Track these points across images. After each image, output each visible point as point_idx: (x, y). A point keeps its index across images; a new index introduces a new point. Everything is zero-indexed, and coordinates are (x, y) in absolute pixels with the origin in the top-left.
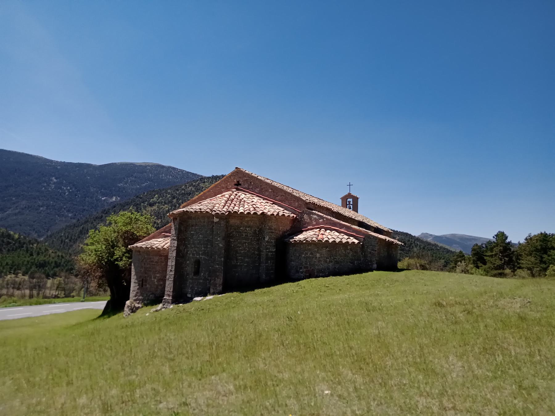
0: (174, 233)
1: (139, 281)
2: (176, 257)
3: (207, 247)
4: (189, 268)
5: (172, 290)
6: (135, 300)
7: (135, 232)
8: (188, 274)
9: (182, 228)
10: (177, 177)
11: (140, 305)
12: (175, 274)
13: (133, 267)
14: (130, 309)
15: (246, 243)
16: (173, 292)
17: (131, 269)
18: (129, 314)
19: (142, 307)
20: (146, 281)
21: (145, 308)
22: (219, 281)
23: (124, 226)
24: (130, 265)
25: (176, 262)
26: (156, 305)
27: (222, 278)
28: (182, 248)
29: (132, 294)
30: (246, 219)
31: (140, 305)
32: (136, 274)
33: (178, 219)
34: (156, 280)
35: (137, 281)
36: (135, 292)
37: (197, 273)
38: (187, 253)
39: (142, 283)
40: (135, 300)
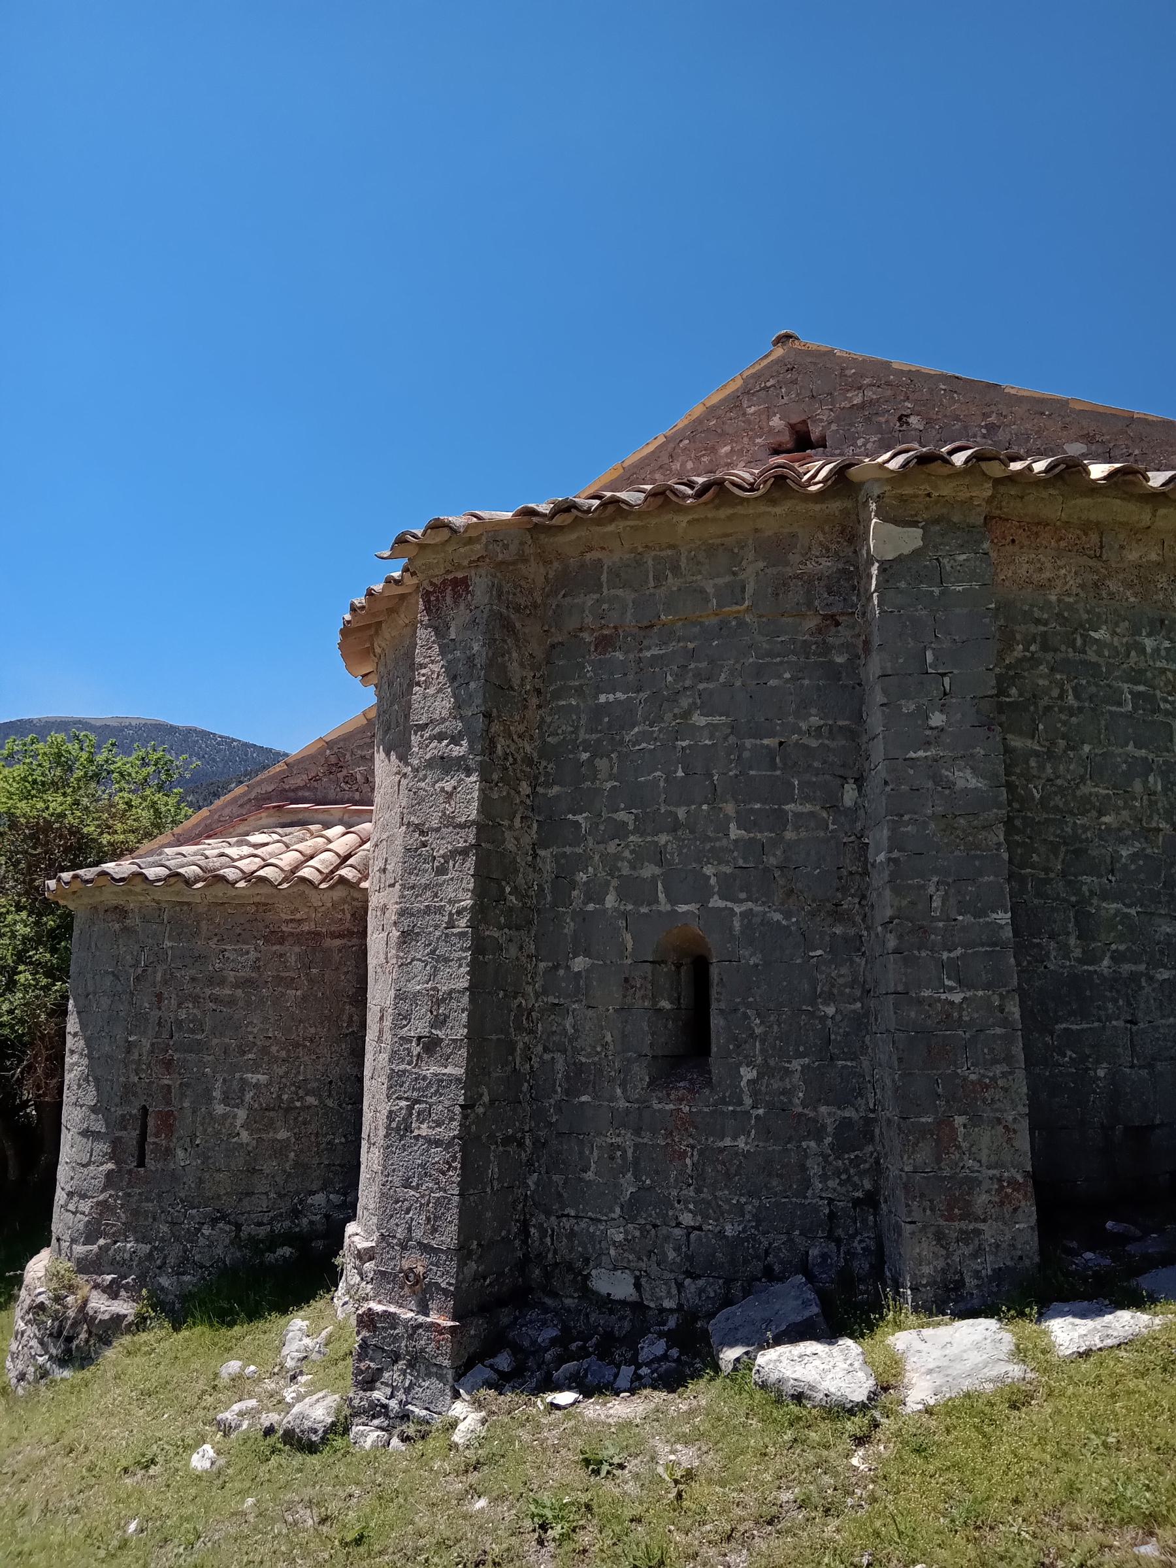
0: (443, 705)
1: (117, 1124)
2: (480, 913)
3: (779, 820)
4: (604, 1020)
5: (448, 1237)
6: (85, 1266)
7: (90, 829)
8: (578, 1077)
9: (515, 671)
10: (214, 760)
11: (124, 1307)
12: (473, 1079)
13: (72, 1024)
14: (56, 1335)
15: (1147, 767)
16: (463, 1251)
17: (62, 1034)
18: (44, 1374)
19: (141, 1323)
20: (168, 1122)
21: (159, 1338)
22: (996, 1148)
23: (27, 796)
24: (60, 1012)
25: (476, 968)
26: (254, 1314)
27: (1016, 1113)
28: (518, 838)
29: (65, 1219)
30: (1132, 556)
31: (124, 1307)
32: (95, 1077)
33: (480, 584)
34: (242, 1114)
35: (99, 1126)
36: (85, 1206)
37: (689, 1048)
38: (563, 879)
39: (136, 1140)
40: (85, 1266)
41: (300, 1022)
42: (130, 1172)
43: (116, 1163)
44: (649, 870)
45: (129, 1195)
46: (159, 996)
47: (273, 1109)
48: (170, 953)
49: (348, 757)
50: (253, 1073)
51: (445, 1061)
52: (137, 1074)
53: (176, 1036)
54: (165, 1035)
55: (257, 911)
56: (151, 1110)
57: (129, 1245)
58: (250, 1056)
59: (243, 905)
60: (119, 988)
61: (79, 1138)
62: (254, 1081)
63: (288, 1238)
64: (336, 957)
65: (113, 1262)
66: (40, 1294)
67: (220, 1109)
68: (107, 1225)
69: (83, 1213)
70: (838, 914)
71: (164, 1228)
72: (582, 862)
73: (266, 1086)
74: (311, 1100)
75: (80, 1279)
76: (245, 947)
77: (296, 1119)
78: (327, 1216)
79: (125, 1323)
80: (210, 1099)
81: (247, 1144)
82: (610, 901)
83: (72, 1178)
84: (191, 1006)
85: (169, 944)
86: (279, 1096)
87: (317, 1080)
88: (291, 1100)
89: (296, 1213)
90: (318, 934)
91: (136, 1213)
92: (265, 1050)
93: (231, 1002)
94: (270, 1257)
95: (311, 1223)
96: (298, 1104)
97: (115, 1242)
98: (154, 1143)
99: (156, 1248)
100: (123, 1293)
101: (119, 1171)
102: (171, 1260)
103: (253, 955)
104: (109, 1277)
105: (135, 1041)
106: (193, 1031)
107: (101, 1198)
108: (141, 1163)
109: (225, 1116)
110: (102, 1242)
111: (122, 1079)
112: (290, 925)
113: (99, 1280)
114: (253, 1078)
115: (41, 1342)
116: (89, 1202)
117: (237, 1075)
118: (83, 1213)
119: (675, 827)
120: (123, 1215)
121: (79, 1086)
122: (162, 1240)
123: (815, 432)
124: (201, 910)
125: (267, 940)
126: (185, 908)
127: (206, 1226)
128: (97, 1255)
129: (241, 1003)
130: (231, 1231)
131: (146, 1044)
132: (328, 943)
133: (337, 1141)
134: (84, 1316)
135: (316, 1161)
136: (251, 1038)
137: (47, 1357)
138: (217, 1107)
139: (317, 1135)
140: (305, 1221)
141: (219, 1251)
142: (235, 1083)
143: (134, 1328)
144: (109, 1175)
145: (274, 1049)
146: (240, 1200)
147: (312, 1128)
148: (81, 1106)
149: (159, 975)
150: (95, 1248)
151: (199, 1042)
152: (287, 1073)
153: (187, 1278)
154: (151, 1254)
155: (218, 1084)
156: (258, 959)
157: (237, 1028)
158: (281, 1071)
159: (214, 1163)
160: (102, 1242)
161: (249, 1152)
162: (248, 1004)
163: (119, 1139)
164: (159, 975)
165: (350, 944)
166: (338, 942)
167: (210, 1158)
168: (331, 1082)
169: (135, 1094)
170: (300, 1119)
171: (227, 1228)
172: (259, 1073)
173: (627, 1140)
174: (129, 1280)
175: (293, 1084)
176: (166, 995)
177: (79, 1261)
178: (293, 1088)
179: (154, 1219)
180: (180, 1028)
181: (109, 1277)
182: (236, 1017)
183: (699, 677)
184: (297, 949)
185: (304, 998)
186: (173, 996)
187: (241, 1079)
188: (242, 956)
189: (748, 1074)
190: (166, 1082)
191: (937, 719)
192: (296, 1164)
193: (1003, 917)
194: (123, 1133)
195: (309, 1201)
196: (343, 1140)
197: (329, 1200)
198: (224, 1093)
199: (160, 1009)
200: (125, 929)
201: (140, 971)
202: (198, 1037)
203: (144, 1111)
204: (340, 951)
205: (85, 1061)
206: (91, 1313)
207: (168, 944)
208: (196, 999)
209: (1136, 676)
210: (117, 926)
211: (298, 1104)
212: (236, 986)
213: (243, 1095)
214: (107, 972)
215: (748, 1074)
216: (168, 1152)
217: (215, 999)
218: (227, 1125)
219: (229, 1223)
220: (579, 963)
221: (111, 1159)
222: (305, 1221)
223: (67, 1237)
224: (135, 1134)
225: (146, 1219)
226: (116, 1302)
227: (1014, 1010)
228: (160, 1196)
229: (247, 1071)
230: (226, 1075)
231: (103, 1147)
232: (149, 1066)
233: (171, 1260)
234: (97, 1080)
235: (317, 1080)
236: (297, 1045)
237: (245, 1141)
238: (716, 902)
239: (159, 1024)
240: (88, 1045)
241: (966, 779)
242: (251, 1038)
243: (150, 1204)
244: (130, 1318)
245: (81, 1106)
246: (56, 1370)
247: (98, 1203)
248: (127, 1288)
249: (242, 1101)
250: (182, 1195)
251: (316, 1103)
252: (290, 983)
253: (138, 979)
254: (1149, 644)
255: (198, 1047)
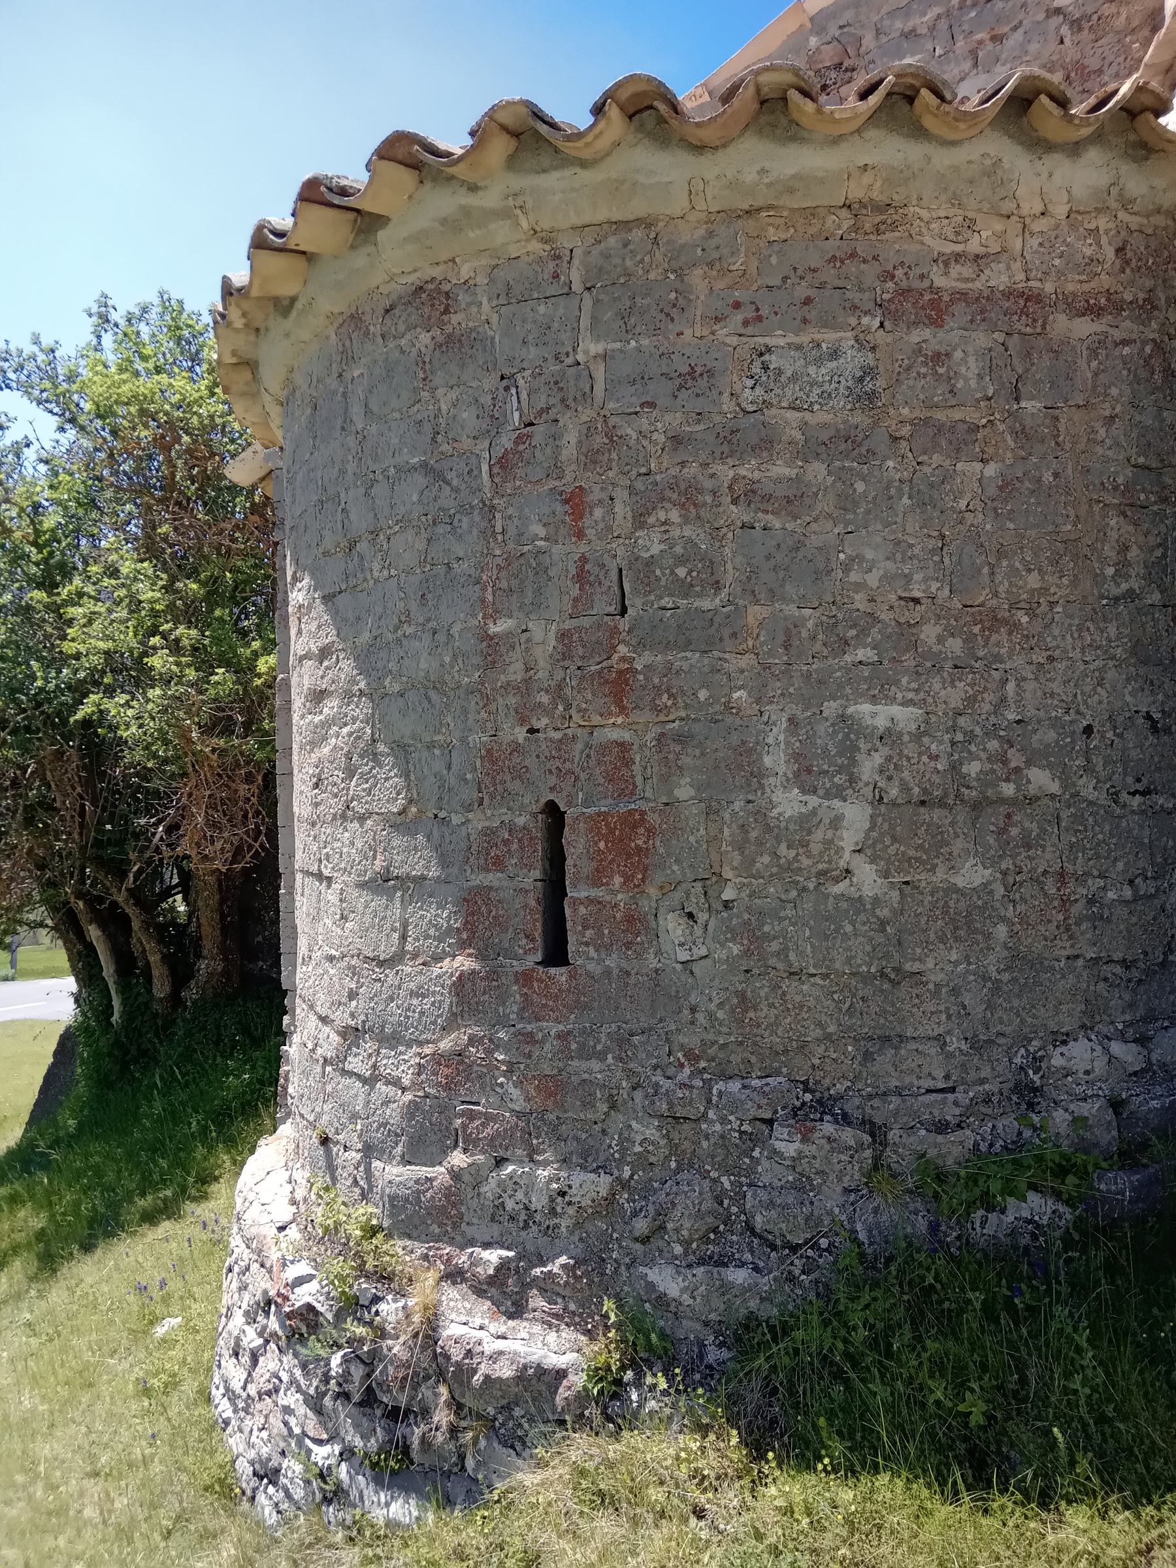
20: (629, 845)
32: (394, 741)
34: (855, 816)
35: (418, 861)
36: (403, 1064)
39: (540, 895)
41: (1001, 554)
42: (525, 978)
43: (481, 956)
45: (530, 1038)
46: (575, 502)
47: (942, 803)
48: (599, 372)
49: (869, 41)
50: (874, 700)
52: (522, 721)
53: (635, 605)
54: (604, 604)
55: (855, 228)
56: (570, 814)
57: (543, 1173)
58: (862, 654)
59: (811, 213)
60: (447, 500)
61: (360, 899)
62: (881, 723)
63: (1022, 1165)
64: (1085, 369)
65: (497, 1212)
66: (300, 1281)
67: (788, 803)
68: (472, 1116)
69: (396, 1082)
71: (647, 1131)
73: (917, 736)
74: (1041, 779)
75: (402, 1253)
76: (828, 337)
77: (1001, 832)
78: (1116, 1105)
79: (562, 1393)
80: (756, 777)
81: (876, 901)
83: (353, 995)
84: (675, 516)
85: (596, 348)
86: (954, 767)
87: (1056, 723)
88: (987, 780)
89: (1028, 1095)
90: (1032, 298)
91: (554, 1088)
92: (906, 635)
93: (794, 501)
94: (990, 1226)
95: (1078, 1121)
96: (1008, 789)
97: (500, 1162)
98: (590, 901)
99: (625, 1185)
100: (537, 1301)
101: (493, 974)
102: (682, 1222)
103: (852, 360)
104: (493, 1256)
105: (509, 634)
106: (686, 589)
107: (445, 1045)
108: (556, 954)
109: (806, 822)
110: (458, 1159)
111: (478, 738)
112: (956, 270)
113: (462, 1259)
114: (877, 715)
115: (315, 1404)
116: (411, 1056)
117: (831, 708)
118: (396, 1082)
120: (515, 1093)
121: (350, 772)
122: (643, 1162)
124: (688, 234)
125: (889, 311)
126: (637, 234)
127: (780, 1131)
128: (448, 1193)
129: (825, 504)
130: (861, 1146)
131: (544, 637)
132: (1062, 324)
133: (1111, 895)
134: (436, 1363)
135: (1063, 949)
136: (860, 601)
137: (337, 1449)
138: (778, 796)
139: (1062, 875)
140: (1060, 1117)
141: (831, 1200)
142: (822, 728)
143: (593, 1411)
144: (462, 984)
145: (929, 633)
146: (868, 1056)
147: (1047, 858)
148: (362, 819)
149: (572, 437)
150: (439, 1172)
151: (709, 619)
152: (971, 700)
153: (738, 1276)
154: (611, 1199)
155: (778, 734)
156: (868, 372)
157: (819, 576)
158: (955, 696)
159: (783, 953)
160: (458, 1159)
161: (883, 924)
162: (847, 502)
163: (484, 891)
164: (572, 437)
165: (1117, 335)
166: (1084, 327)
167: (769, 938)
168: (1088, 730)
169: (519, 773)
170: (1014, 831)
171: (848, 1136)
172: (893, 700)
174: (554, 1268)
175: (992, 732)
176: (596, 494)
177: (395, 1204)
178: (993, 745)
179: (613, 1107)
180: (647, 582)
181: (493, 1256)
182: (814, 541)
184: (982, 339)
185: (1006, 486)
186: (621, 495)
187: (843, 718)
188: (819, 362)
190: (615, 735)
192: (1015, 958)
194: (492, 878)
195: (1057, 1061)
196: (1128, 893)
197: (1111, 1059)
198: (797, 757)
199: (580, 535)
200: (450, 343)
201: (506, 441)
202: (706, 604)
203: (554, 816)
204: (1093, 353)
205: (361, 709)
206: (457, 1354)
207: (590, 347)
208: (688, 497)
210: (425, 338)
211: (1008, 789)
212: (807, 452)
213: (853, 762)
214: (405, 470)
216: (635, 927)
217: (747, 494)
218: (815, 848)
219: (845, 1119)
221: (463, 945)
222: (1060, 1117)
223: (351, 1135)
224: (532, 877)
225: (588, 1103)
226: (523, 1328)
228: (622, 1041)
229: (859, 696)
230: (795, 709)
231: (436, 915)
232: (558, 692)
233: (682, 1222)
234: (401, 749)
235: (1056, 723)
236: (994, 622)
237: (868, 892)
239: (581, 577)
240: (364, 668)
242: (860, 601)
243: (595, 1065)
244: (578, 1380)
245: (362, 819)
246: (369, 1493)
247: (439, 1059)
248: (547, 1286)
249: (852, 780)
250: (691, 1040)
251: (1055, 788)
252: (964, 440)
253: (504, 464)
255: (709, 634)
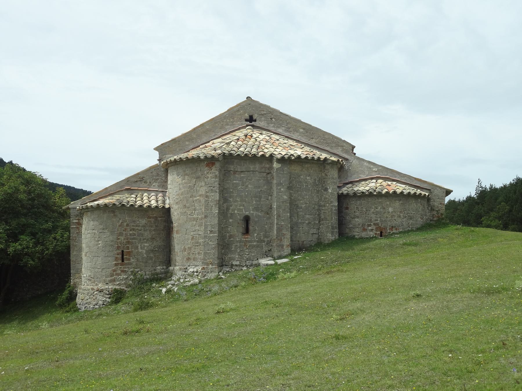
8: (231, 236)
34: (144, 251)
44: (242, 208)
51: (214, 233)
67: (140, 251)
70: (268, 214)
72: (231, 206)
74: (156, 249)
82: (236, 212)
114: (146, 245)
119: (246, 201)
123: (254, 118)
173: (238, 244)
183: (249, 180)
189: (255, 235)
191: (282, 189)
193: (289, 214)
203: (123, 251)
209: (306, 183)
215: (255, 235)
216: (129, 259)
220: (231, 220)
227: (289, 226)
238: (252, 212)
241: (285, 197)
254: (308, 178)
